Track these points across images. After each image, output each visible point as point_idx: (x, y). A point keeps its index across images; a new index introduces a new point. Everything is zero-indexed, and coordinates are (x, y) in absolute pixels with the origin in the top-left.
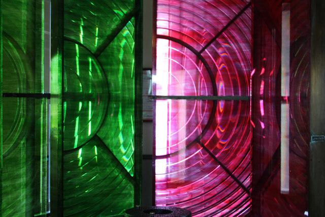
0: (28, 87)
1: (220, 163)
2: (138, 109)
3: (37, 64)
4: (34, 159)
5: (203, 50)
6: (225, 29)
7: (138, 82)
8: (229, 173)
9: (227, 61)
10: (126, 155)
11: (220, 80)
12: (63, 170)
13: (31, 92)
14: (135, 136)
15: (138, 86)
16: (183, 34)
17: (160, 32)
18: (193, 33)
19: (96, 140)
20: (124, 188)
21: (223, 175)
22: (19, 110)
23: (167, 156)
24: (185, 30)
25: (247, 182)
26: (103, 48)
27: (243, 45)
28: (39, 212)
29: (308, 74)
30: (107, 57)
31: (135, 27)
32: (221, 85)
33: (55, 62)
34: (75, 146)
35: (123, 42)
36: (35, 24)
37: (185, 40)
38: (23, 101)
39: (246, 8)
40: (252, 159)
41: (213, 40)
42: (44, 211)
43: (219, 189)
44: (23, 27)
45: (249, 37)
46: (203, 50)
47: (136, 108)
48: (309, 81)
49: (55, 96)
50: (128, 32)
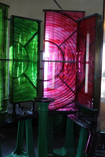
2: (38, 65)
6: (68, 39)
7: (38, 56)
10: (34, 80)
14: (37, 74)
15: (38, 57)
17: (46, 39)
19: (24, 75)
21: (66, 87)
25: (74, 90)
26: (27, 44)
27: (74, 44)
28: (5, 98)
30: (28, 47)
33: (11, 48)
34: (18, 77)
35: (34, 43)
37: (54, 42)
42: (7, 98)
45: (76, 42)
47: (37, 64)
49: (11, 60)
50: (35, 39)
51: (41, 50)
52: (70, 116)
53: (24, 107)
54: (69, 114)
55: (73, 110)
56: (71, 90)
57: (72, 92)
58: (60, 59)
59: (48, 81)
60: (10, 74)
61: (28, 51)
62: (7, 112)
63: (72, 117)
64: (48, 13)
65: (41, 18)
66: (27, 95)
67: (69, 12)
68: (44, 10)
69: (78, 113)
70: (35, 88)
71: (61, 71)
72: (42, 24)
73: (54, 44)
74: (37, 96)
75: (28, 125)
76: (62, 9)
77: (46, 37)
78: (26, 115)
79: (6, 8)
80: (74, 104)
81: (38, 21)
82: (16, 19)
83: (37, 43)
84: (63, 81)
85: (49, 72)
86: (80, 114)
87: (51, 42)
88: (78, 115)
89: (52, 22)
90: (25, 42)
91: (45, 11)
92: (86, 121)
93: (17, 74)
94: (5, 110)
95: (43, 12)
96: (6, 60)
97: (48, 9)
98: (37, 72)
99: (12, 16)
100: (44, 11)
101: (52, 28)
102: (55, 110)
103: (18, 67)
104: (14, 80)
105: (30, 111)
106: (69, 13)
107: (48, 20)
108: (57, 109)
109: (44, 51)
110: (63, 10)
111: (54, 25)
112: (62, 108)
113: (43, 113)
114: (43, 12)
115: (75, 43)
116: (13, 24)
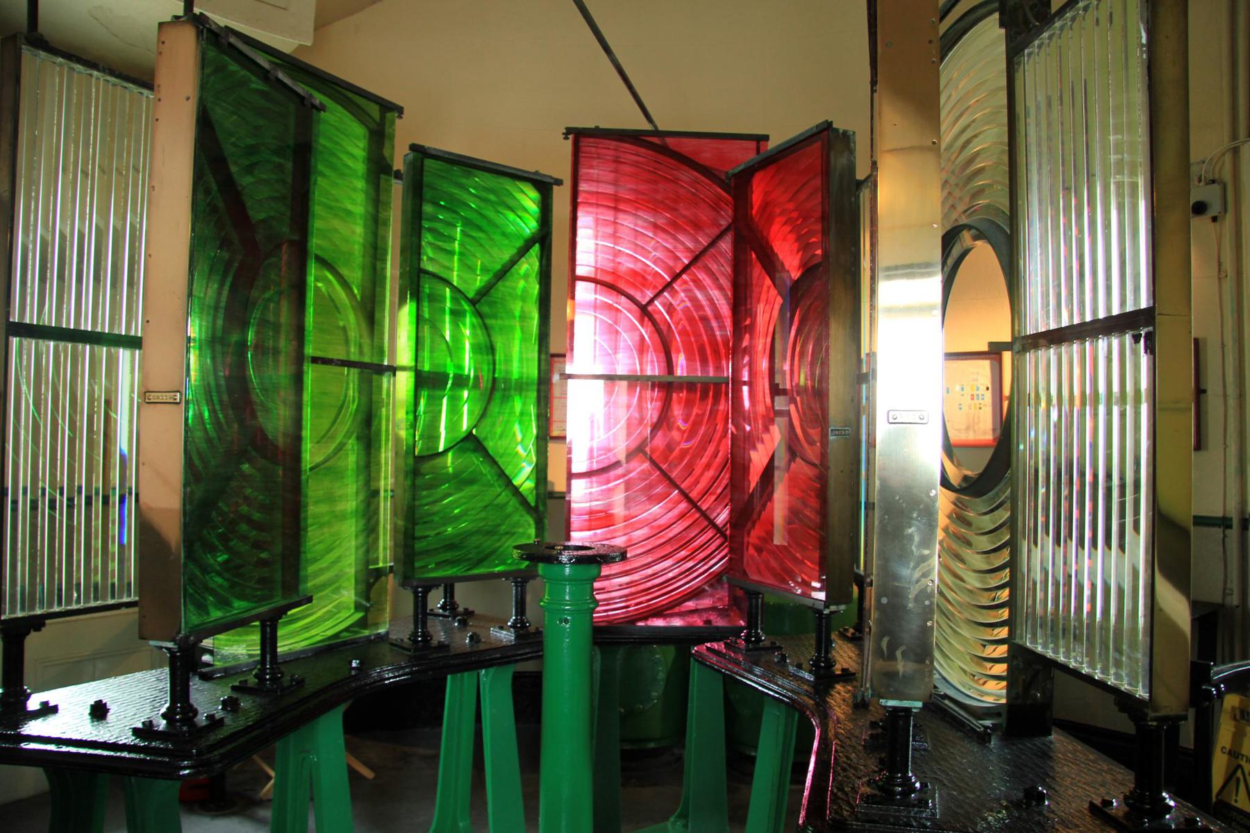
0: (361, 353)
1: (677, 487)
2: (542, 394)
3: (377, 315)
4: (368, 467)
5: (651, 301)
6: (686, 269)
8: (693, 504)
9: (686, 310)
11: (678, 352)
12: (414, 499)
13: (367, 359)
14: (537, 437)
16: (619, 277)
17: (580, 271)
18: (634, 273)
19: (471, 443)
20: (517, 525)
21: (683, 506)
22: (347, 389)
23: (588, 474)
24: (622, 269)
25: (722, 517)
26: (485, 292)
27: (715, 293)
29: (827, 325)
30: (492, 304)
31: (540, 284)
32: (681, 361)
33: (407, 314)
35: (522, 284)
36: (375, 251)
37: (622, 285)
38: (354, 373)
39: (720, 237)
40: (731, 479)
41: (668, 286)
43: (677, 529)
44: (357, 249)
45: (725, 283)
46: (651, 301)
47: (539, 391)
48: (828, 335)
50: (530, 265)
51: (553, 349)
52: (705, 652)
53: (472, 612)
54: (700, 640)
55: (719, 622)
56: (706, 523)
57: (710, 534)
58: (653, 369)
59: (594, 479)
60: (397, 439)
61: (488, 322)
62: (387, 633)
63: (717, 653)
64: (584, 142)
65: (557, 163)
66: (488, 544)
67: (694, 141)
68: (569, 131)
69: (748, 636)
70: (528, 513)
71: (655, 427)
72: (561, 197)
73: (621, 292)
74: (537, 536)
75: (495, 689)
76: (655, 127)
77: (580, 257)
78: (482, 647)
79: (389, 115)
80: (723, 593)
81: (543, 182)
82: (429, 163)
83: (537, 287)
84: (664, 474)
85: (594, 418)
86: (759, 640)
87: (608, 282)
88: (747, 640)
89: (609, 190)
90: (479, 282)
91: (578, 136)
92: (791, 669)
93: (438, 437)
94: (376, 625)
95: (566, 138)
96: (380, 370)
97: (590, 124)
98: (535, 431)
99: (414, 148)
100: (571, 137)
101: (609, 216)
102: (632, 620)
103: (445, 400)
104: (426, 467)
105: (501, 628)
106: (687, 146)
107: (591, 180)
108: (641, 620)
109: (572, 349)
110: (661, 128)
111: (616, 204)
112: (659, 612)
113: (566, 621)
114: (566, 138)
115: (721, 288)
116: (417, 191)
